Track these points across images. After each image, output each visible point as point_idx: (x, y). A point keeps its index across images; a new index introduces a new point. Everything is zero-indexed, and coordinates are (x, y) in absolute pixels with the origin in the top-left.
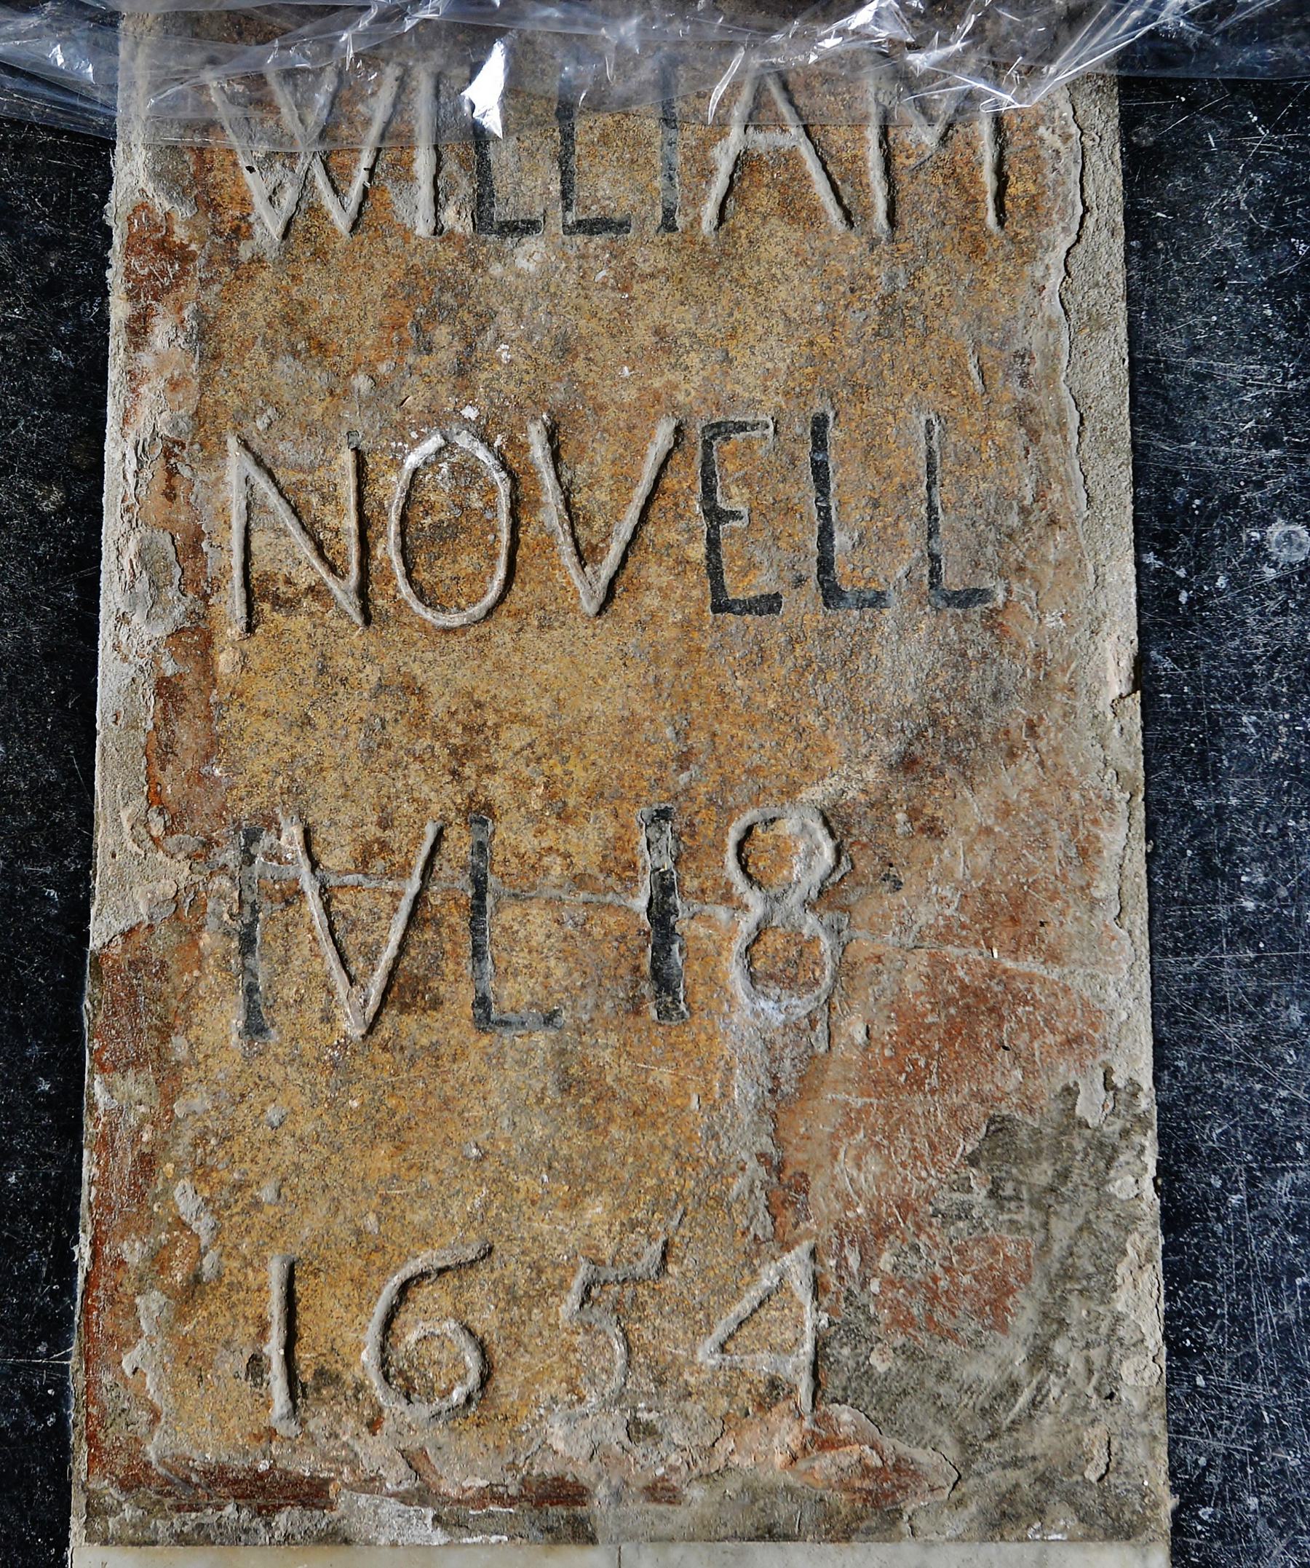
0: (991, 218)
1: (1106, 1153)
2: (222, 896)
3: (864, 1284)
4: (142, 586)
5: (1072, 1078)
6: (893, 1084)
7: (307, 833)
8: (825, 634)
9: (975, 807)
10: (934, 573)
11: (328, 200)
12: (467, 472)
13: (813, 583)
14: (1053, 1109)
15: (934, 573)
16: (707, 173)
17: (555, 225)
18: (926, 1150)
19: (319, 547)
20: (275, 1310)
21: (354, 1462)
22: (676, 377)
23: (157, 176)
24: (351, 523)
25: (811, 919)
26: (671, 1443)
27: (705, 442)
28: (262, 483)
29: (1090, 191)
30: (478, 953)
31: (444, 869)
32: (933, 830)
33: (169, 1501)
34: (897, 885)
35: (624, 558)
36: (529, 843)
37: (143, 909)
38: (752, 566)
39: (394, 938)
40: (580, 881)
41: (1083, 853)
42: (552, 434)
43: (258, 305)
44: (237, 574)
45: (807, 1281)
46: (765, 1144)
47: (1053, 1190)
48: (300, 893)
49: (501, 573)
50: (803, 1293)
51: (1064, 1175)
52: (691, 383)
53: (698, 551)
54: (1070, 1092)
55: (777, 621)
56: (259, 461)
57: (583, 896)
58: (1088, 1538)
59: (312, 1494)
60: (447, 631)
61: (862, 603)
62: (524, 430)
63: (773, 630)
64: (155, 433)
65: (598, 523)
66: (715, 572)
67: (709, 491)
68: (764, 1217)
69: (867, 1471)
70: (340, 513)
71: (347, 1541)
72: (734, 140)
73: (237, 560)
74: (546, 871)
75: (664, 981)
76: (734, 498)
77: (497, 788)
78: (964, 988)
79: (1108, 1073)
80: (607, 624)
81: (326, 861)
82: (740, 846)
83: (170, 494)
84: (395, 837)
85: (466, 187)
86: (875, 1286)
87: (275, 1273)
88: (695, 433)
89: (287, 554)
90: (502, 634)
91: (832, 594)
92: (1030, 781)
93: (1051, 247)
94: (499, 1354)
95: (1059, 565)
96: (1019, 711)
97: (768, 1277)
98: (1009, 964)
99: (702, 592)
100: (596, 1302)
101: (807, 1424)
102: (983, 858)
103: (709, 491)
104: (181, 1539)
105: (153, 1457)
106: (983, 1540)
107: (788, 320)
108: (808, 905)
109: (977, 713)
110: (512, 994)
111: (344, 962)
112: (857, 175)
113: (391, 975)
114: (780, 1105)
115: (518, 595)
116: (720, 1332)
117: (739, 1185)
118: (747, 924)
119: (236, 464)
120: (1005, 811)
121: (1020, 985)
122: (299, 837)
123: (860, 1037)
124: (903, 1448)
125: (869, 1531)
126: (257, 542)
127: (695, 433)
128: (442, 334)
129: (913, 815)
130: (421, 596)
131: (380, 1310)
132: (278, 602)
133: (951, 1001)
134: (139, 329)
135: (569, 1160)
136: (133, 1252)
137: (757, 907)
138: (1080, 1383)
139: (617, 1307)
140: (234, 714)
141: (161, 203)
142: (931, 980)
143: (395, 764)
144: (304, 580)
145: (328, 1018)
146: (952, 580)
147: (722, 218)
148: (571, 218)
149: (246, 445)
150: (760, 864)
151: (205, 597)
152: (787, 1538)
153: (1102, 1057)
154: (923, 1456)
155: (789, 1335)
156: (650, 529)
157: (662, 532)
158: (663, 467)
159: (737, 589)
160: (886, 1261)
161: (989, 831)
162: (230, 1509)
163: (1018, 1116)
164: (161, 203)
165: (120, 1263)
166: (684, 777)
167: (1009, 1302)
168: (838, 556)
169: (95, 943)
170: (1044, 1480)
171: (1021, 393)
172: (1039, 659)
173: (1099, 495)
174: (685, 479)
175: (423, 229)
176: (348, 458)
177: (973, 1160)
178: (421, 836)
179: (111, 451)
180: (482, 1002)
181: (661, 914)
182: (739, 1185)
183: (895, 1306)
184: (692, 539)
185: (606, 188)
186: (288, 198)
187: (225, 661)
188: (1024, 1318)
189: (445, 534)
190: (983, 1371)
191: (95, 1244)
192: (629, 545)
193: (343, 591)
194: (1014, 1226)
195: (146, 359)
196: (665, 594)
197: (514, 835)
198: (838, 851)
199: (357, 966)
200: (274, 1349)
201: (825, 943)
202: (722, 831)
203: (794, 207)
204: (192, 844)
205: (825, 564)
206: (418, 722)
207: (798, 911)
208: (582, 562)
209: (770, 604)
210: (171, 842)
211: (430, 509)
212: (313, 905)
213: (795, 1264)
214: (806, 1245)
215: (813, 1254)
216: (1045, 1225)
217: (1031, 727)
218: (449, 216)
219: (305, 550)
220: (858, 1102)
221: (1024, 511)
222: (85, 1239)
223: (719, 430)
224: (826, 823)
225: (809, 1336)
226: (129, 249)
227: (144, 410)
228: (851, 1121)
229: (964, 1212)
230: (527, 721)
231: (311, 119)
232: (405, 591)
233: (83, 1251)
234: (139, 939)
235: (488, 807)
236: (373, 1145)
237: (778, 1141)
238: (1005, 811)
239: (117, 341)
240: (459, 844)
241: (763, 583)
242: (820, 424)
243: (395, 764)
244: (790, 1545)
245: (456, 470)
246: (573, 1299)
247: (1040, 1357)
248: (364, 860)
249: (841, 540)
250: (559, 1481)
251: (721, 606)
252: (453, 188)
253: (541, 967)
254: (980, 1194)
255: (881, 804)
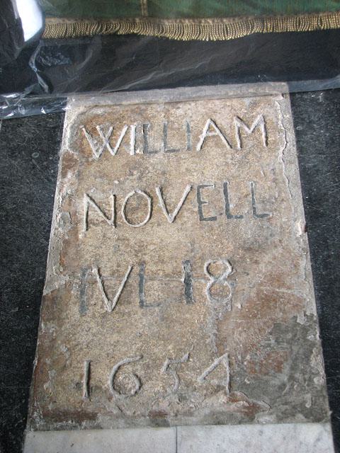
0: (265, 145)
1: (305, 330)
2: (76, 283)
3: (243, 363)
4: (62, 223)
5: (295, 315)
6: (249, 317)
7: (99, 271)
8: (228, 224)
9: (267, 258)
10: (254, 211)
11: (110, 149)
12: (141, 198)
13: (224, 214)
14: (291, 321)
15: (254, 211)
16: (198, 140)
17: (162, 152)
18: (258, 332)
19: (105, 214)
20: (85, 373)
21: (104, 408)
22: (191, 177)
23: (70, 147)
24: (113, 209)
25: (226, 282)
26: (191, 401)
27: (198, 190)
28: (92, 203)
29: (287, 139)
30: (141, 291)
31: (133, 275)
32: (256, 262)
33: (53, 420)
34: (248, 274)
35: (178, 212)
36: (154, 268)
37: (57, 287)
38: (209, 212)
39: (120, 290)
40: (167, 276)
41: (295, 266)
42: (161, 190)
43: (92, 169)
44: (85, 220)
45: (227, 363)
46: (215, 331)
47: (292, 339)
48: (96, 282)
49: (148, 216)
50: (226, 365)
51: (295, 335)
52: (195, 179)
53: (196, 209)
54: (295, 317)
55: (216, 222)
56: (91, 199)
57: (168, 279)
58: (309, 422)
59: (92, 417)
60: (145, 224)
61: (236, 217)
62: (154, 188)
63: (215, 224)
64: (67, 194)
65: (172, 205)
66: (200, 212)
67: (199, 198)
68: (215, 348)
69: (245, 407)
70: (110, 207)
71: (101, 428)
72: (204, 134)
73: (85, 217)
74: (159, 274)
75: (188, 295)
76: (204, 198)
77: (147, 258)
78: (266, 295)
79: (305, 312)
80: (175, 224)
81: (103, 275)
82: (207, 268)
83: (70, 205)
84: (121, 269)
85: (141, 146)
86: (245, 363)
87: (85, 364)
88: (196, 187)
89: (97, 215)
90: (149, 228)
91: (229, 216)
92: (281, 252)
93: (279, 149)
94: (144, 380)
95: (285, 209)
96: (277, 238)
97: (216, 362)
98: (277, 290)
99: (197, 217)
100: (170, 368)
101: (228, 396)
102: (270, 268)
103: (199, 198)
104: (57, 429)
105: (50, 409)
106: (278, 423)
107: (217, 166)
108: (225, 279)
109: (267, 239)
110: (148, 300)
111: (107, 295)
112: (233, 138)
113: (119, 299)
114: (218, 323)
115: (152, 220)
116: (204, 374)
117: (208, 341)
118: (209, 284)
119: (86, 200)
120: (275, 258)
121: (280, 294)
122: (97, 271)
123: (240, 307)
124: (255, 401)
125: (246, 422)
126: (90, 213)
127: (196, 187)
128: (135, 172)
129: (251, 259)
130: (129, 222)
131: (113, 372)
132: (94, 224)
133: (263, 299)
134: (64, 175)
135: (163, 335)
136: (48, 361)
137: (212, 280)
138: (303, 383)
139: (176, 369)
140: (82, 246)
141: (71, 152)
142: (258, 294)
143: (121, 254)
144: (100, 219)
145: (102, 307)
146: (259, 212)
147: (201, 148)
148: (166, 150)
149: (88, 195)
150: (212, 270)
151: (77, 224)
152: (223, 424)
153: (304, 309)
154: (261, 403)
155: (223, 375)
156: (185, 206)
157: (187, 206)
158: (188, 195)
159: (205, 215)
160: (248, 357)
161: (271, 262)
162: (70, 422)
163: (282, 323)
164: (71, 152)
165: (45, 364)
166: (193, 254)
167: (282, 365)
168: (231, 210)
169: (44, 294)
170: (294, 407)
171: (274, 177)
172: (281, 227)
173: (294, 194)
174: (194, 197)
175: (132, 153)
176: (112, 197)
177: (271, 334)
178: (128, 268)
179: (56, 197)
180: (142, 302)
181: (187, 283)
182: (208, 341)
183: (252, 368)
184: (195, 207)
185: (174, 144)
186: (100, 151)
187: (80, 236)
188: (286, 369)
189: (136, 209)
190: (276, 382)
191: (39, 361)
192: (180, 210)
193: (111, 222)
194: (283, 348)
195: (66, 180)
196: (188, 218)
197: (151, 267)
198: (232, 269)
199: (110, 296)
200: (84, 381)
201: (230, 287)
202: (203, 264)
203: (218, 144)
204: (70, 273)
205: (227, 210)
206: (127, 246)
207: (223, 281)
208: (168, 212)
209: (214, 219)
210: (65, 273)
211: (132, 205)
212: (100, 284)
213: (224, 360)
214: (227, 354)
215: (229, 356)
216: (291, 347)
217: (280, 241)
218: (138, 151)
219: (101, 214)
220: (240, 321)
221: (276, 199)
222: (36, 359)
223: (200, 187)
224: (229, 263)
225: (228, 375)
226: (63, 160)
227: (65, 189)
228: (238, 325)
229: (269, 345)
230: (154, 244)
231: (106, 136)
232: (125, 221)
233: (36, 362)
234: (55, 292)
235: (144, 262)
236: (112, 334)
237: (218, 330)
238: (275, 258)
239: (59, 177)
240: (137, 269)
241: (213, 214)
242: (225, 185)
243: (121, 254)
244: (224, 426)
245: (138, 198)
246: (163, 369)
247: (291, 378)
248: (113, 274)
249: (231, 206)
250: (160, 412)
251: (202, 219)
252: (138, 145)
253: (157, 294)
254: (273, 341)
255: (243, 258)
